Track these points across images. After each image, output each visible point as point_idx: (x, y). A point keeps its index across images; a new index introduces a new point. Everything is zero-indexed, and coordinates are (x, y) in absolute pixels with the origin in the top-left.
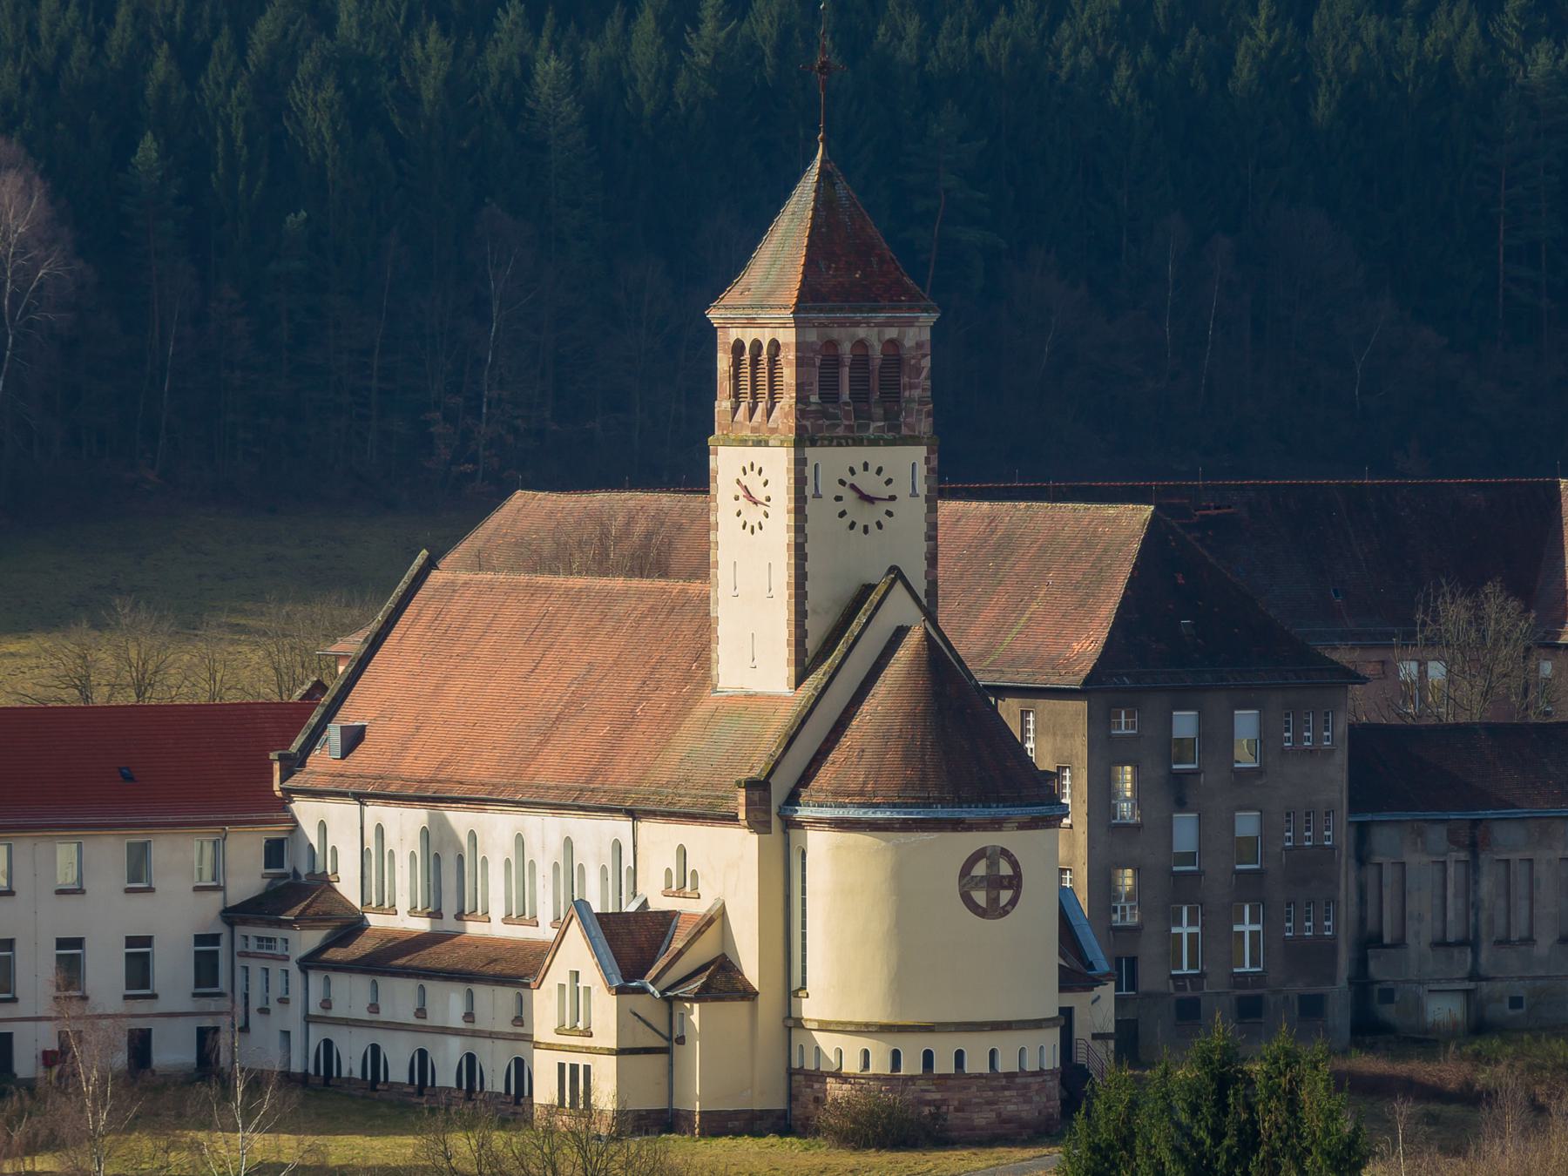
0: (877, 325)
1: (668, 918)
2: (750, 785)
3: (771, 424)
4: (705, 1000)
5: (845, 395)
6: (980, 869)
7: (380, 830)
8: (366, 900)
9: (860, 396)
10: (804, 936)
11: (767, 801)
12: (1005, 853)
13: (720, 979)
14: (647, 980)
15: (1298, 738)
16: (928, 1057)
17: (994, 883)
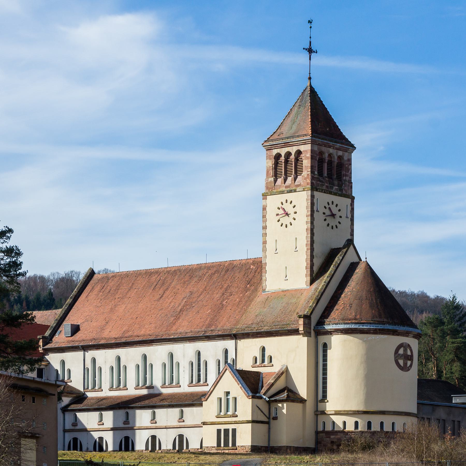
0: (337, 149)
3: (297, 183)
4: (288, 401)
6: (401, 351)
7: (94, 360)
9: (330, 176)
11: (310, 324)
12: (409, 345)
13: (292, 396)
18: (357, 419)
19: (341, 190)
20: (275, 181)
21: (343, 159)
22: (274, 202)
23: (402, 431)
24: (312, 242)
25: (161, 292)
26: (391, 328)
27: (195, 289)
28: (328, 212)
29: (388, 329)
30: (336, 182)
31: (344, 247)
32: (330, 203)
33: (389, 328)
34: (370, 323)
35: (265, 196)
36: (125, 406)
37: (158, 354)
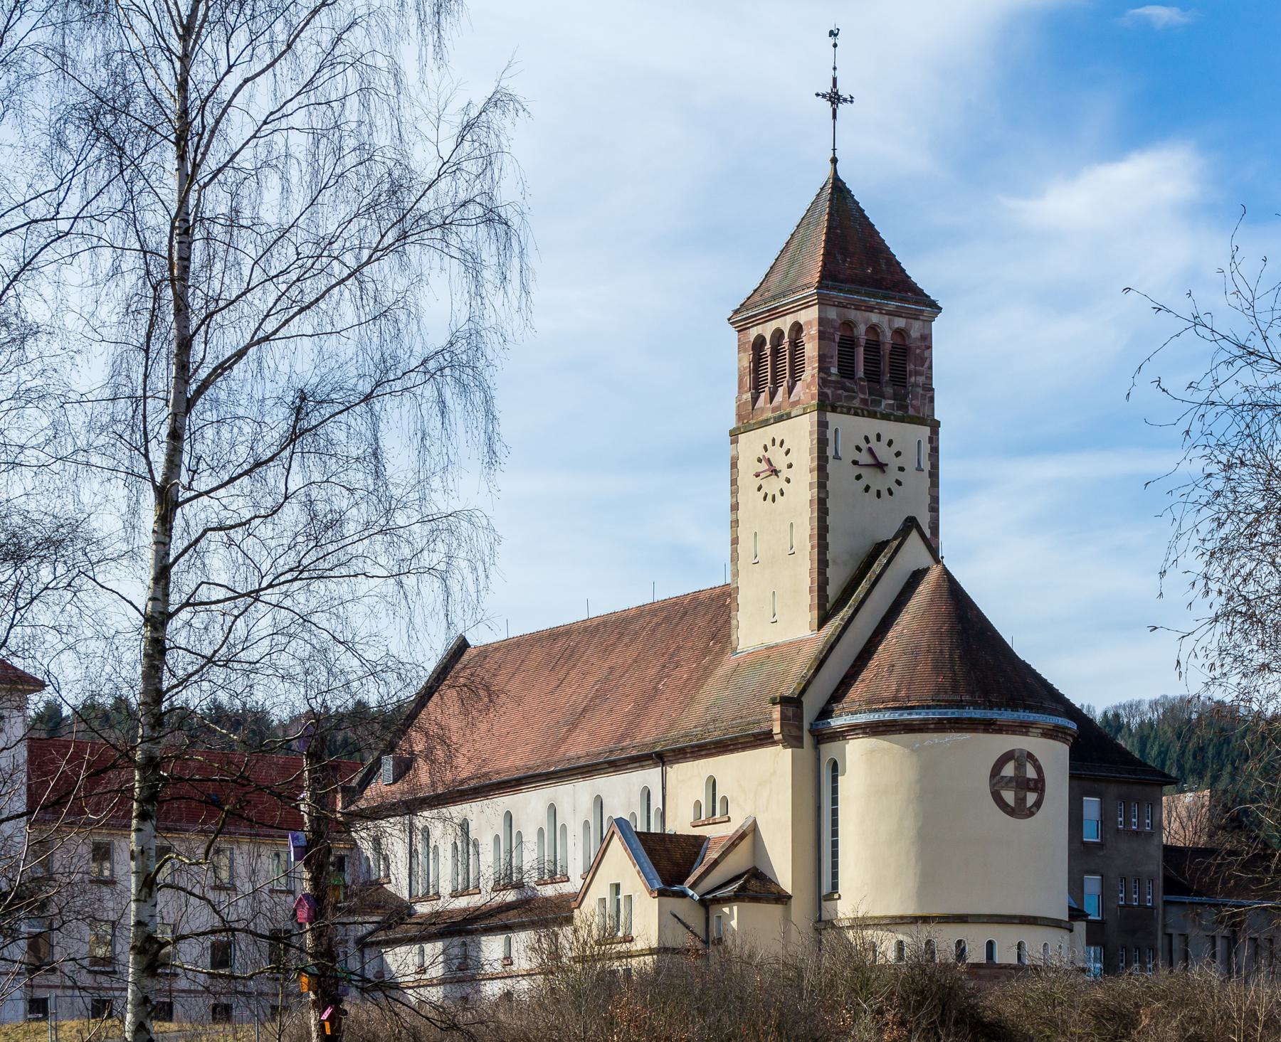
0: (889, 313)
1: (697, 844)
2: (784, 701)
4: (743, 900)
5: (860, 373)
6: (1009, 770)
8: (414, 893)
9: (873, 376)
10: (835, 844)
11: (799, 717)
12: (1030, 756)
13: (755, 885)
14: (686, 885)
15: (1127, 822)
17: (1022, 784)
18: (900, 937)
19: (903, 407)
20: (755, 399)
21: (909, 336)
22: (752, 443)
23: (1014, 960)
24: (823, 530)
25: (563, 672)
26: (978, 716)
27: (620, 661)
28: (865, 458)
29: (970, 719)
30: (889, 390)
31: (895, 538)
32: (873, 438)
33: (974, 716)
34: (929, 707)
35: (734, 435)
36: (462, 928)
37: (529, 805)
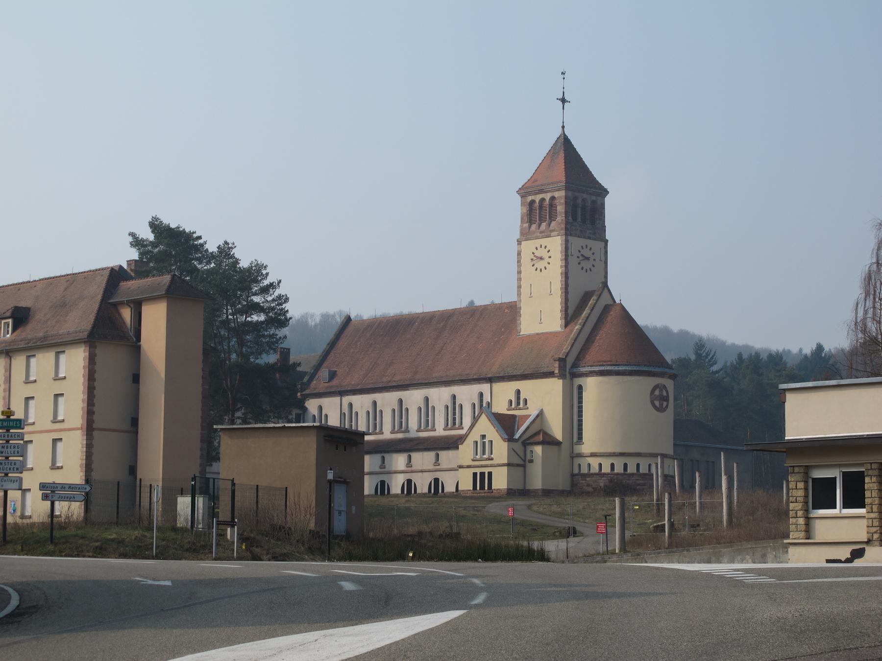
2: (560, 360)
6: (657, 392)
9: (584, 221)
16: (625, 465)
22: (529, 247)
